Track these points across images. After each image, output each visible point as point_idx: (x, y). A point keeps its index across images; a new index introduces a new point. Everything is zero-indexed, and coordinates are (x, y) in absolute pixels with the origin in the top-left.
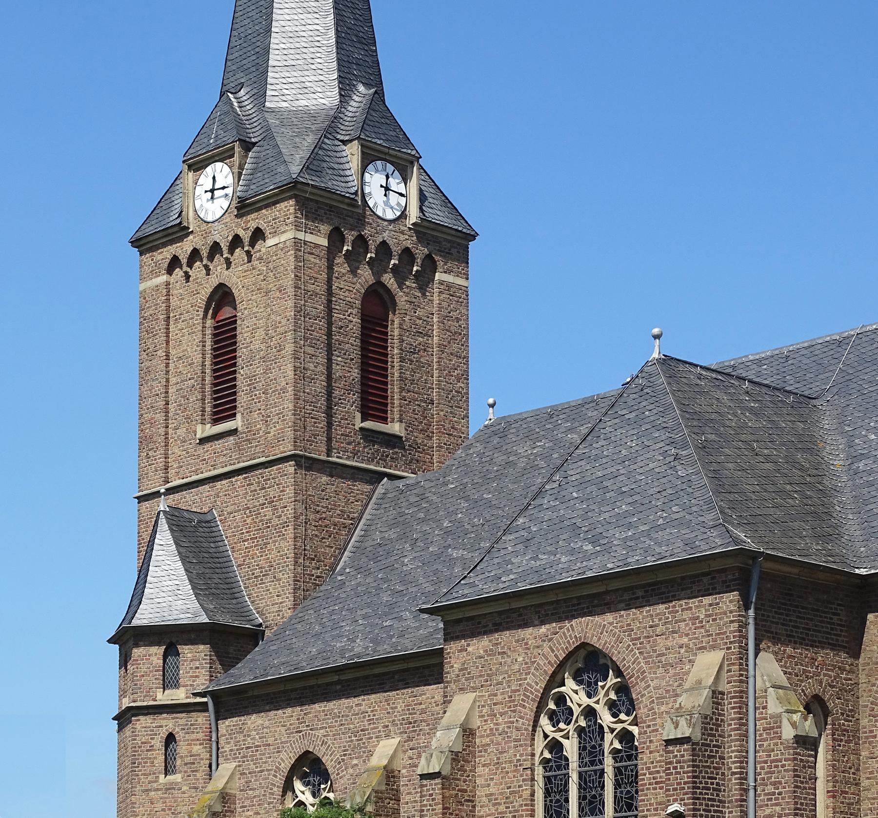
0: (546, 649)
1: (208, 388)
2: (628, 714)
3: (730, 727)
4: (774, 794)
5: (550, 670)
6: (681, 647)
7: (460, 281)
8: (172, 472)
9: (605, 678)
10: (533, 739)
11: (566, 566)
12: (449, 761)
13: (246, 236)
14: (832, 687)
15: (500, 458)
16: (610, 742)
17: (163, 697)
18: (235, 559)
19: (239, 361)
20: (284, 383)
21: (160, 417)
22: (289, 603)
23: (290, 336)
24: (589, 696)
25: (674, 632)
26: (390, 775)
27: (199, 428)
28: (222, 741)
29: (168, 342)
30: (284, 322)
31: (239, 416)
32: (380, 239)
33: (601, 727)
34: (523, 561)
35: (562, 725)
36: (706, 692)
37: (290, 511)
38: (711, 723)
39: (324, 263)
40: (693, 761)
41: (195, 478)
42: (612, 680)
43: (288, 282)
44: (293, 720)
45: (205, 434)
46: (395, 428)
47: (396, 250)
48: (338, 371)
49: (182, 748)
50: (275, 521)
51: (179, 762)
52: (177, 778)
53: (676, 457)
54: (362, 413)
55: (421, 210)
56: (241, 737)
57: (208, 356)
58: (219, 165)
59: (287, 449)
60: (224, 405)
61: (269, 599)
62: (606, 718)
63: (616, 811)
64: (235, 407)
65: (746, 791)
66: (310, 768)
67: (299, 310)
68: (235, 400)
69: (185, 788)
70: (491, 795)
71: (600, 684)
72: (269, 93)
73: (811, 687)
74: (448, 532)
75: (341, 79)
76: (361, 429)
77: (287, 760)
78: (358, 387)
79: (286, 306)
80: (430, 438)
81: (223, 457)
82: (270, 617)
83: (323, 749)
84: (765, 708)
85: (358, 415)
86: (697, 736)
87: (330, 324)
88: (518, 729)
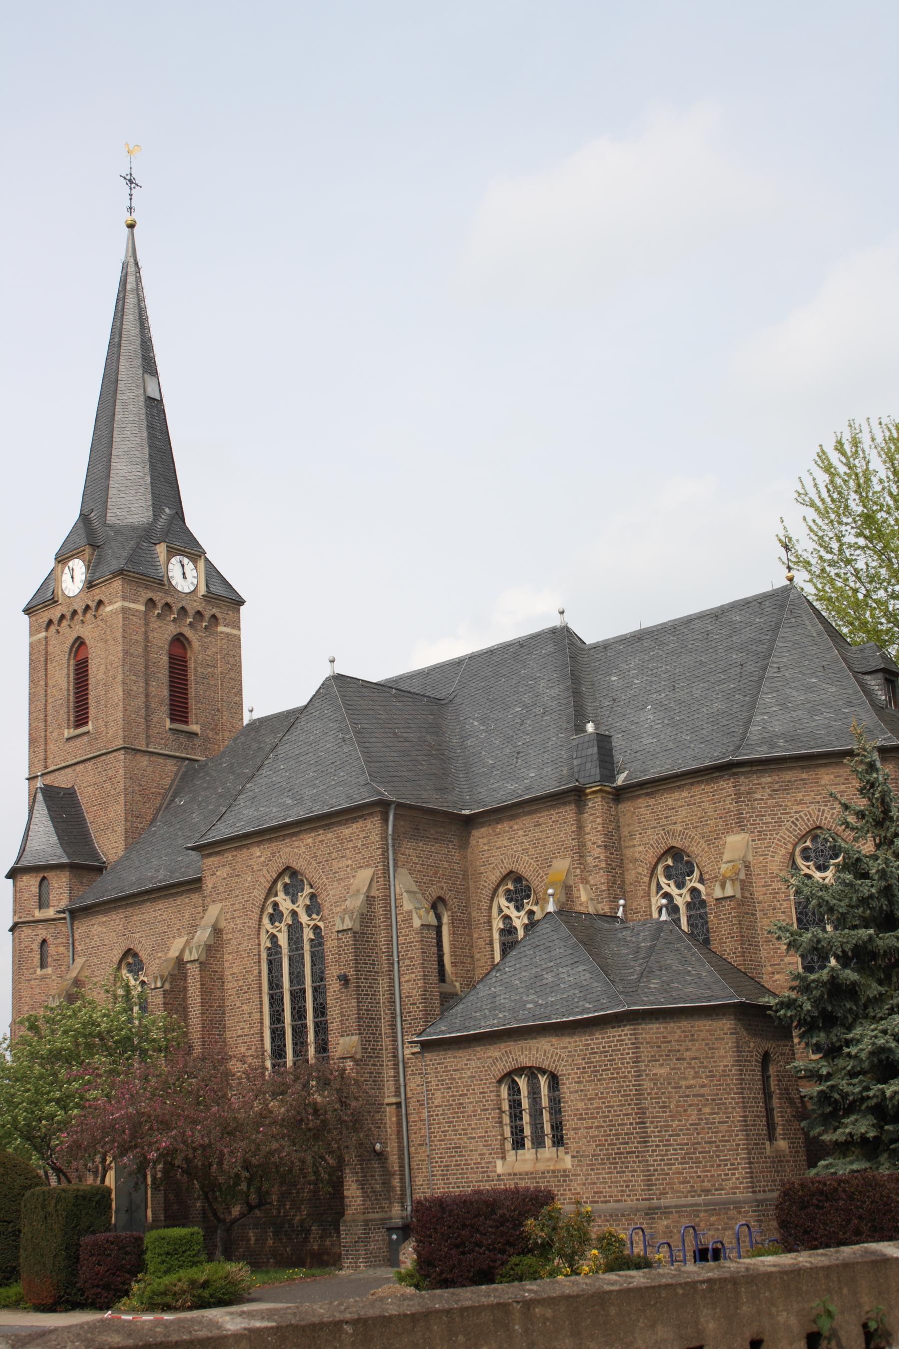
0: (265, 871)
1: (72, 705)
2: (318, 915)
3: (380, 921)
4: (410, 965)
5: (268, 885)
6: (347, 867)
7: (234, 632)
8: (49, 761)
9: (302, 890)
10: (259, 934)
11: (275, 816)
12: (205, 951)
13: (93, 605)
14: (450, 890)
15: (255, 746)
16: (308, 934)
17: (38, 915)
18: (89, 817)
19: (90, 687)
20: (116, 701)
21: (42, 725)
22: (122, 847)
23: (120, 669)
24: (293, 902)
25: (343, 857)
26: (180, 962)
27: (66, 732)
28: (77, 943)
29: (46, 676)
30: (117, 660)
31: (90, 723)
32: (180, 605)
33: (301, 924)
34: (250, 812)
35: (277, 924)
36: (362, 897)
37: (122, 785)
38: (366, 918)
39: (142, 622)
40: (355, 944)
41: (63, 765)
42: (307, 890)
43: (119, 634)
44: (120, 927)
45: (71, 735)
46: (195, 728)
47: (191, 612)
48: (153, 690)
49: (52, 950)
50: (113, 792)
51: (49, 960)
52: (49, 970)
53: (344, 740)
54: (171, 719)
55: (207, 587)
56: (88, 940)
57: (72, 684)
58: (77, 560)
59: (120, 743)
60: (81, 717)
61: (110, 844)
62: (304, 918)
63: (313, 982)
64: (88, 717)
65: (393, 964)
66: (131, 959)
67: (126, 653)
68: (87, 713)
69: (54, 977)
70: (234, 974)
71: (525, 901)
72: (108, 515)
73: (434, 892)
74: (221, 796)
75: (154, 505)
76: (170, 729)
77: (117, 954)
78: (167, 702)
79: (118, 650)
80: (218, 734)
81: (81, 748)
82: (111, 857)
83: (139, 947)
84: (402, 906)
85: (168, 720)
86: (357, 928)
87: (147, 661)
88: (249, 927)
